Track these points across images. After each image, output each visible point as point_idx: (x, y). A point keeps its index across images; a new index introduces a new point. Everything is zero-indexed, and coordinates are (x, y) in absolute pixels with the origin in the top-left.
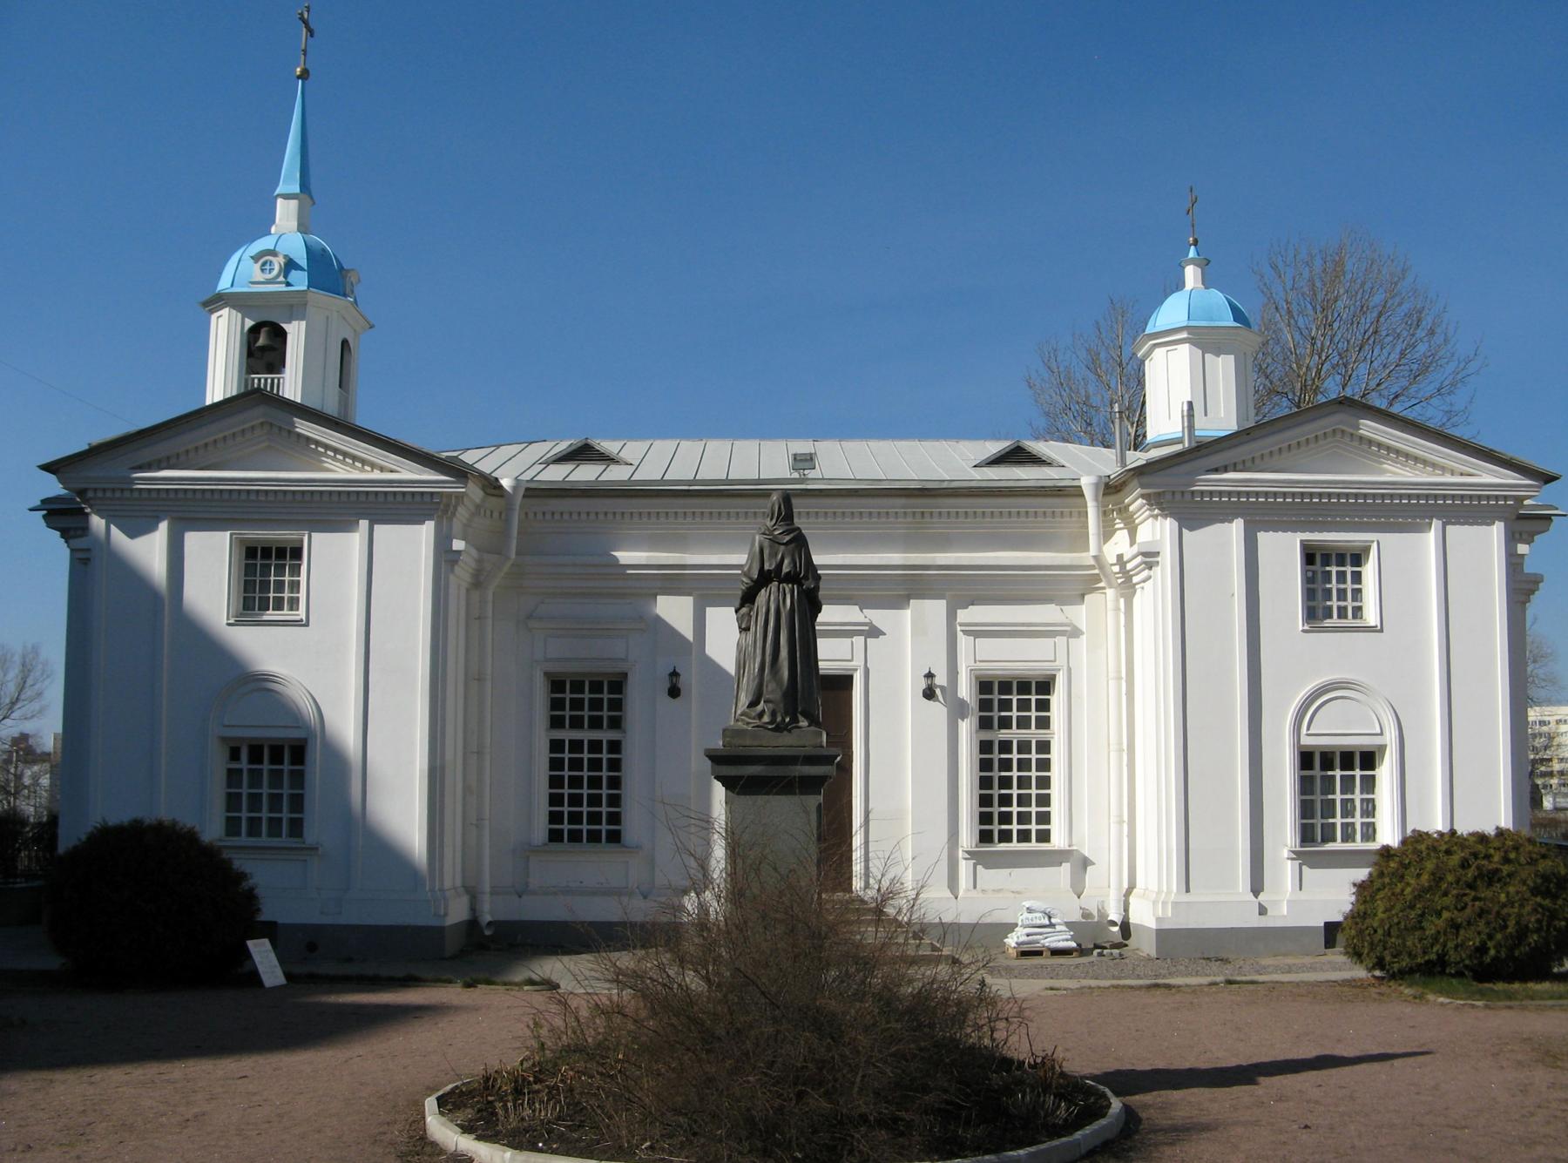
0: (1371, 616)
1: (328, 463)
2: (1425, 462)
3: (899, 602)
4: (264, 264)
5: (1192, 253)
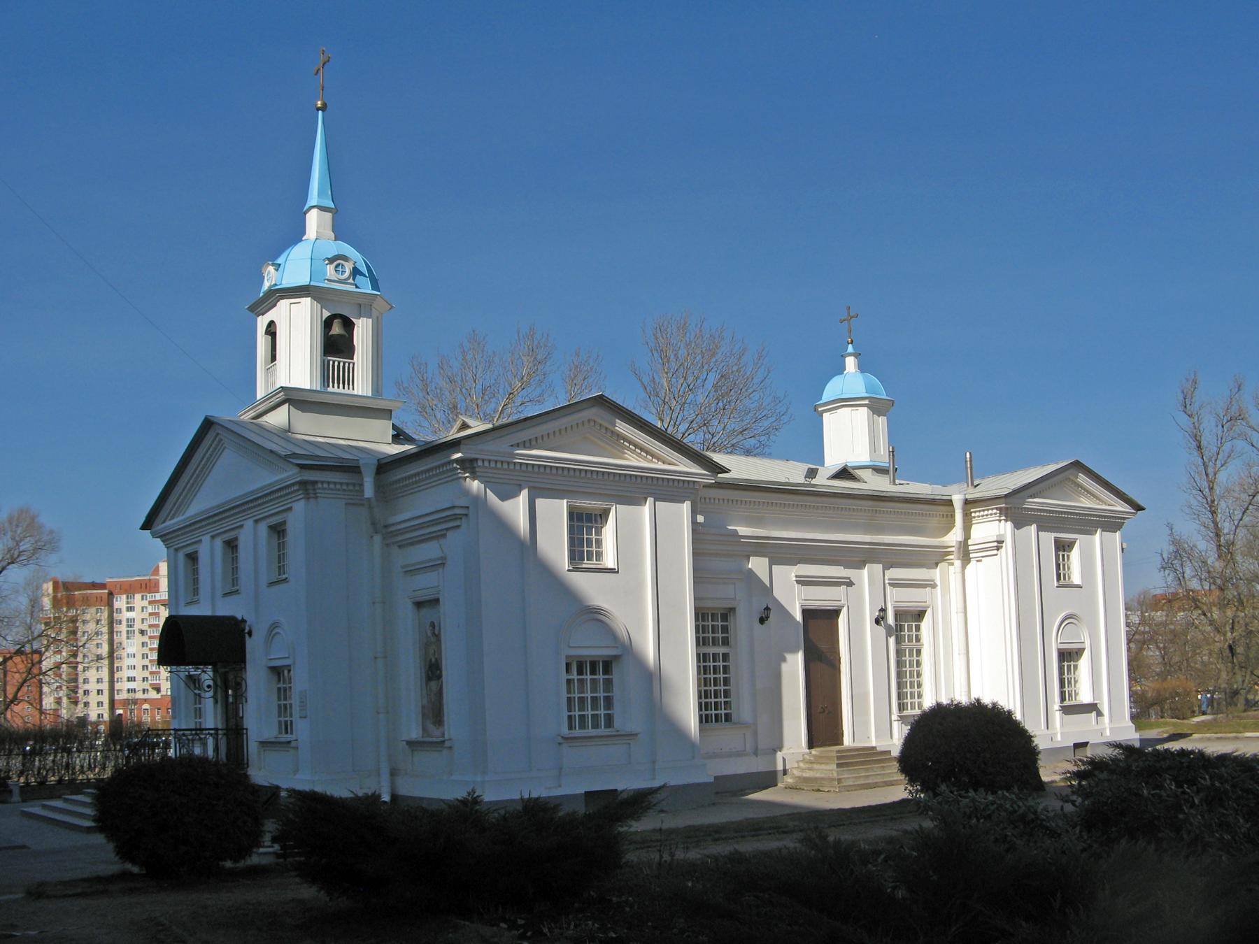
0: (609, 561)
1: (628, 454)
2: (1094, 496)
3: (860, 565)
4: (337, 266)
5: (850, 349)
